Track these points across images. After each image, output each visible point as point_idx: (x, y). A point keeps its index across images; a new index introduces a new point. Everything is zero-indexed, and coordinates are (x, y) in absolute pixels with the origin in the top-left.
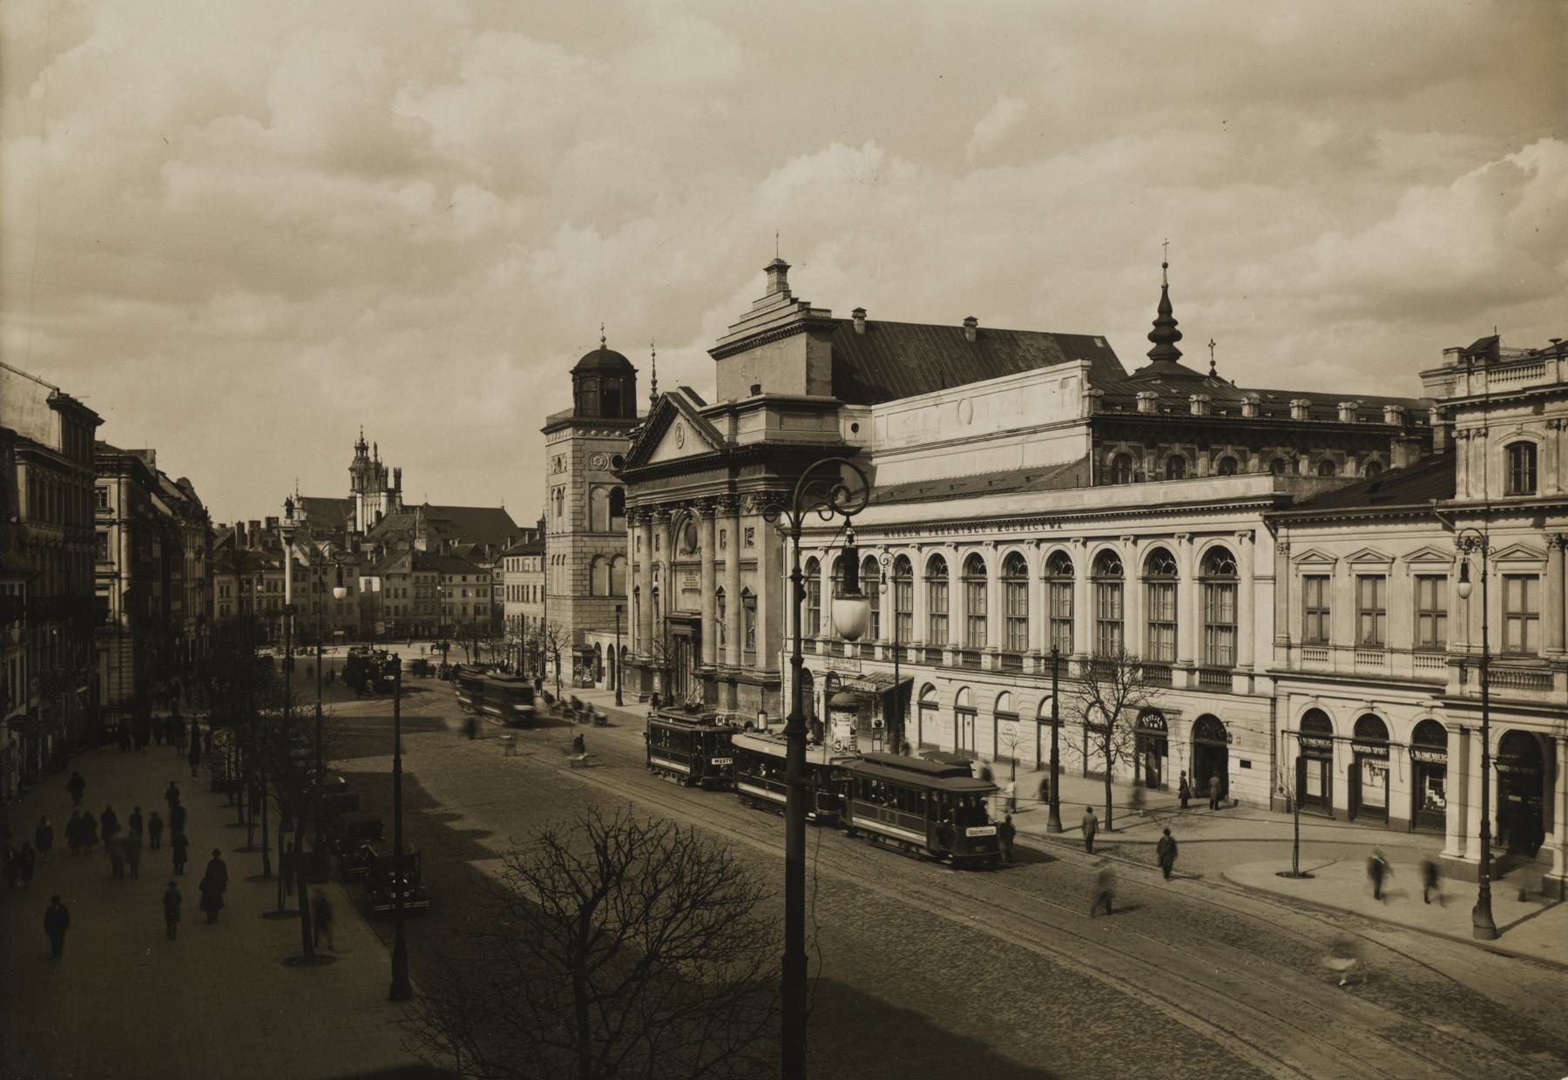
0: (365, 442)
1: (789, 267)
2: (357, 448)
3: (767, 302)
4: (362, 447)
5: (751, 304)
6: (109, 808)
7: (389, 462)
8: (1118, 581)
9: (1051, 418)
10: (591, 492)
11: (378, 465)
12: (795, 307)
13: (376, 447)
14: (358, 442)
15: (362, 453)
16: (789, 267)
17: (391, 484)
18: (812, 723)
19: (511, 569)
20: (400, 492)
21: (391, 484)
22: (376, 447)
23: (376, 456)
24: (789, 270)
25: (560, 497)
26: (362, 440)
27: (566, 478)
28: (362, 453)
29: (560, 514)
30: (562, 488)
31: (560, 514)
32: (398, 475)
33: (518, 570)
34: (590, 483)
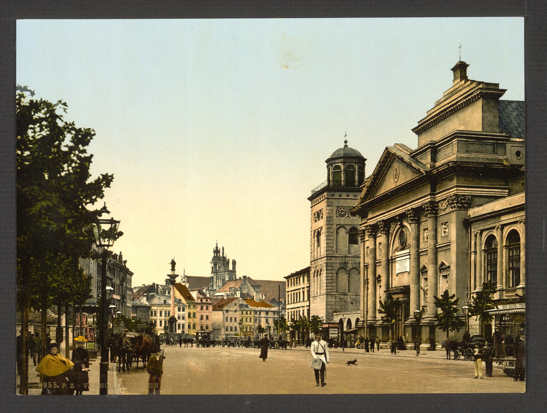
0: (218, 248)
1: (468, 65)
2: (214, 252)
3: (436, 108)
4: (217, 251)
5: (417, 123)
6: (506, 90)
7: (230, 256)
8: (518, 246)
9: (218, 314)
10: (338, 229)
11: (224, 258)
12: (474, 85)
13: (223, 249)
14: (215, 248)
15: (217, 254)
16: (468, 65)
17: (231, 268)
18: (100, 230)
19: (295, 301)
20: (235, 272)
21: (231, 268)
22: (223, 249)
23: (223, 253)
24: (468, 68)
25: (319, 234)
26: (217, 247)
27: (322, 223)
28: (217, 254)
29: (319, 245)
30: (320, 230)
31: (319, 245)
32: (234, 263)
33: (299, 301)
34: (337, 225)
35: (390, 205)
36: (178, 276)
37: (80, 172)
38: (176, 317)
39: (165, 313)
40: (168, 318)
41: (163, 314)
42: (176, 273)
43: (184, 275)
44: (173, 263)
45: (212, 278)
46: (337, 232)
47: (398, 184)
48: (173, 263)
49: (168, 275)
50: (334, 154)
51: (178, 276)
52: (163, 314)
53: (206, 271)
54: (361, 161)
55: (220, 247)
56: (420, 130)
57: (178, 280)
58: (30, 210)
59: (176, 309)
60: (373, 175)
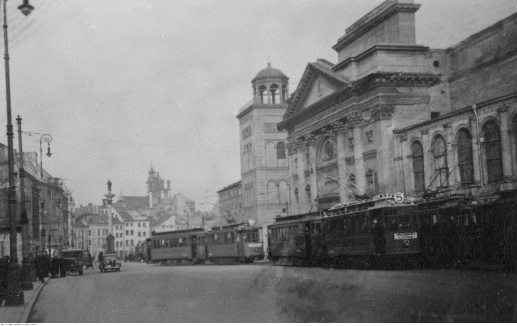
2: (149, 173)
4: (152, 172)
7: (164, 176)
32: (169, 182)
35: (390, 115)
36: (114, 196)
37: (52, 273)
38: (115, 235)
39: (103, 232)
40: (106, 237)
41: (101, 233)
42: (113, 193)
43: (121, 195)
44: (110, 184)
45: (148, 197)
46: (266, 148)
47: (322, 97)
48: (110, 184)
49: (105, 195)
50: (260, 73)
51: (114, 196)
52: (101, 233)
53: (143, 191)
54: (285, 79)
55: (156, 170)
56: (339, 47)
57: (115, 200)
58: (288, 116)
59: (114, 227)
60: (297, 91)
